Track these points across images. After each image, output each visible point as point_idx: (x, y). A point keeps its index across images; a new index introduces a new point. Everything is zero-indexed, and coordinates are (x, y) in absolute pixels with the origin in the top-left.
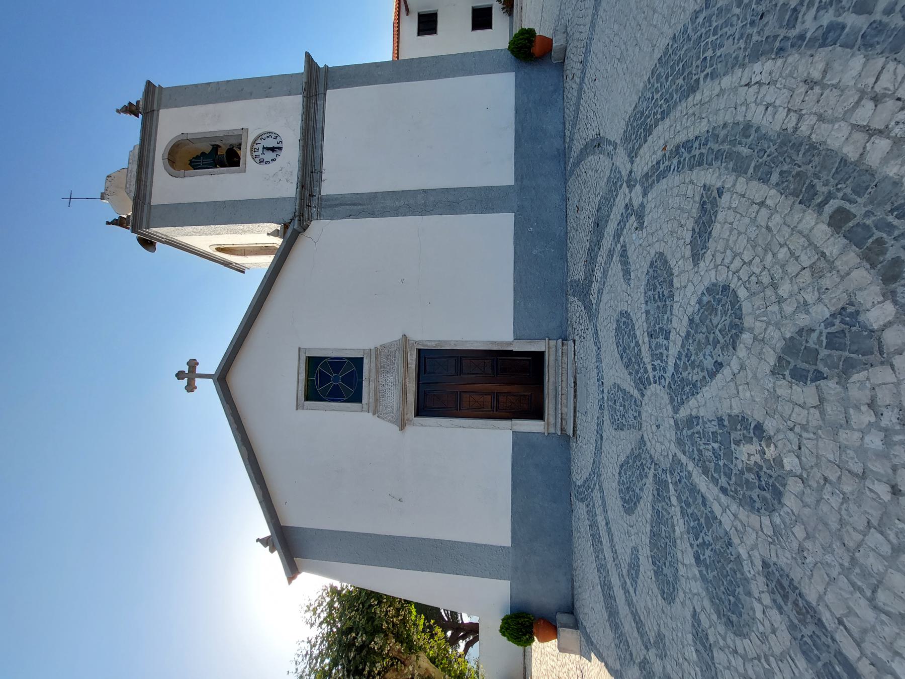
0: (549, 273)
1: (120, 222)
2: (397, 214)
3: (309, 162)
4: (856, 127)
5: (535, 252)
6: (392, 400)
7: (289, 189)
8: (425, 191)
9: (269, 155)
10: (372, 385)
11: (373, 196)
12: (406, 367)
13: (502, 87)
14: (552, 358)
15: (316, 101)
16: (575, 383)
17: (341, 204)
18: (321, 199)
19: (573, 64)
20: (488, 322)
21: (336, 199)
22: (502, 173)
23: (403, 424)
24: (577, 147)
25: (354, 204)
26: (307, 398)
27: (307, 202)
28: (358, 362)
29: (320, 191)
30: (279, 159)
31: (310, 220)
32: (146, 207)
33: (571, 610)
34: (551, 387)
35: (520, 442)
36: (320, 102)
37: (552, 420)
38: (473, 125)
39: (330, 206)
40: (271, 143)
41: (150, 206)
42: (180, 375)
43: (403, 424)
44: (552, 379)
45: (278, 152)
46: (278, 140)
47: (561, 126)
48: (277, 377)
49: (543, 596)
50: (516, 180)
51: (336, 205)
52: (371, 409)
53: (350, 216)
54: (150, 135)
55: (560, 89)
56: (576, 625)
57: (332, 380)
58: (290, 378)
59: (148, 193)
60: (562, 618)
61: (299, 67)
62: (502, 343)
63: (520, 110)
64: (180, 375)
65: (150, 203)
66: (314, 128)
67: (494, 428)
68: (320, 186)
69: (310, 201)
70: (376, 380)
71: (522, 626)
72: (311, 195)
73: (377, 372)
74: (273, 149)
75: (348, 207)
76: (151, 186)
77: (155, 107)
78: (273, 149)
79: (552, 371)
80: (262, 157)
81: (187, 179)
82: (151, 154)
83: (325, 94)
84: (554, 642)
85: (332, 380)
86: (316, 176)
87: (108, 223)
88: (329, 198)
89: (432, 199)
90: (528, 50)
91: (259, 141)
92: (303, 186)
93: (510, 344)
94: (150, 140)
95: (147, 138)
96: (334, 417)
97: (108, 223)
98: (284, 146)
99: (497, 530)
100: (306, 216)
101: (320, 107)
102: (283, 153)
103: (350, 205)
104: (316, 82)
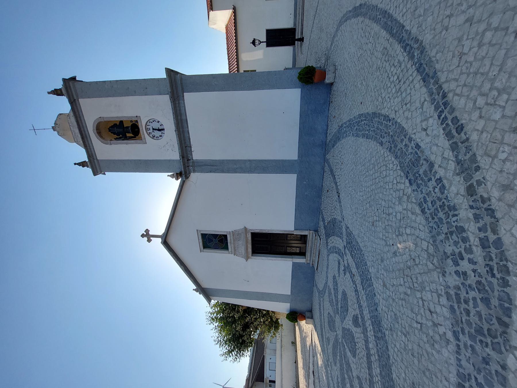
0: (311, 198)
1: (83, 164)
2: (236, 172)
3: (183, 142)
4: (496, 29)
5: (306, 193)
6: (242, 250)
7: (175, 155)
8: (249, 160)
9: (157, 133)
10: (232, 245)
11: (222, 162)
12: (246, 237)
13: (292, 98)
14: (311, 237)
15: (179, 101)
16: (319, 254)
17: (205, 165)
18: (193, 162)
19: (338, 87)
20: (281, 220)
21: (202, 162)
22: (291, 153)
23: (247, 259)
24: (333, 129)
25: (213, 166)
26: (202, 234)
27: (187, 165)
28: (225, 236)
29: (192, 157)
30: (165, 136)
31: (190, 173)
32: (95, 160)
33: (311, 311)
34: (309, 247)
35: (294, 264)
36: (181, 102)
37: (309, 259)
38: (275, 120)
39: (200, 166)
40: (156, 126)
41: (98, 160)
42: (143, 236)
43: (247, 259)
44: (310, 245)
45: (163, 131)
46: (160, 124)
47: (325, 127)
48: (189, 244)
49: (300, 307)
50: (299, 157)
51: (202, 165)
52: (233, 252)
53: (211, 172)
54: (80, 118)
55: (328, 102)
56: (312, 317)
57: (214, 242)
58: (197, 242)
59: (93, 153)
60: (308, 314)
61: (163, 75)
62: (289, 231)
63: (304, 115)
64: (143, 236)
65: (97, 159)
66: (181, 120)
67: (285, 260)
68: (192, 155)
69: (188, 163)
70: (234, 244)
71: (294, 316)
72: (188, 160)
73: (234, 241)
74: (159, 130)
75: (209, 167)
76: (88, 131)
77: (75, 97)
78: (159, 130)
79: (310, 242)
80: (153, 133)
81: (113, 146)
82: (85, 128)
83: (183, 96)
84: (305, 321)
85: (214, 242)
86: (188, 148)
87: (49, 93)
88: (198, 161)
89: (254, 165)
90: (310, 77)
91: (148, 124)
92: (183, 158)
93: (292, 231)
94: (81, 120)
95: (79, 119)
96: (216, 256)
97: (75, 164)
98: (165, 127)
99: (286, 290)
100: (188, 172)
101: (182, 105)
102: (165, 131)
103: (210, 165)
104: (176, 85)
